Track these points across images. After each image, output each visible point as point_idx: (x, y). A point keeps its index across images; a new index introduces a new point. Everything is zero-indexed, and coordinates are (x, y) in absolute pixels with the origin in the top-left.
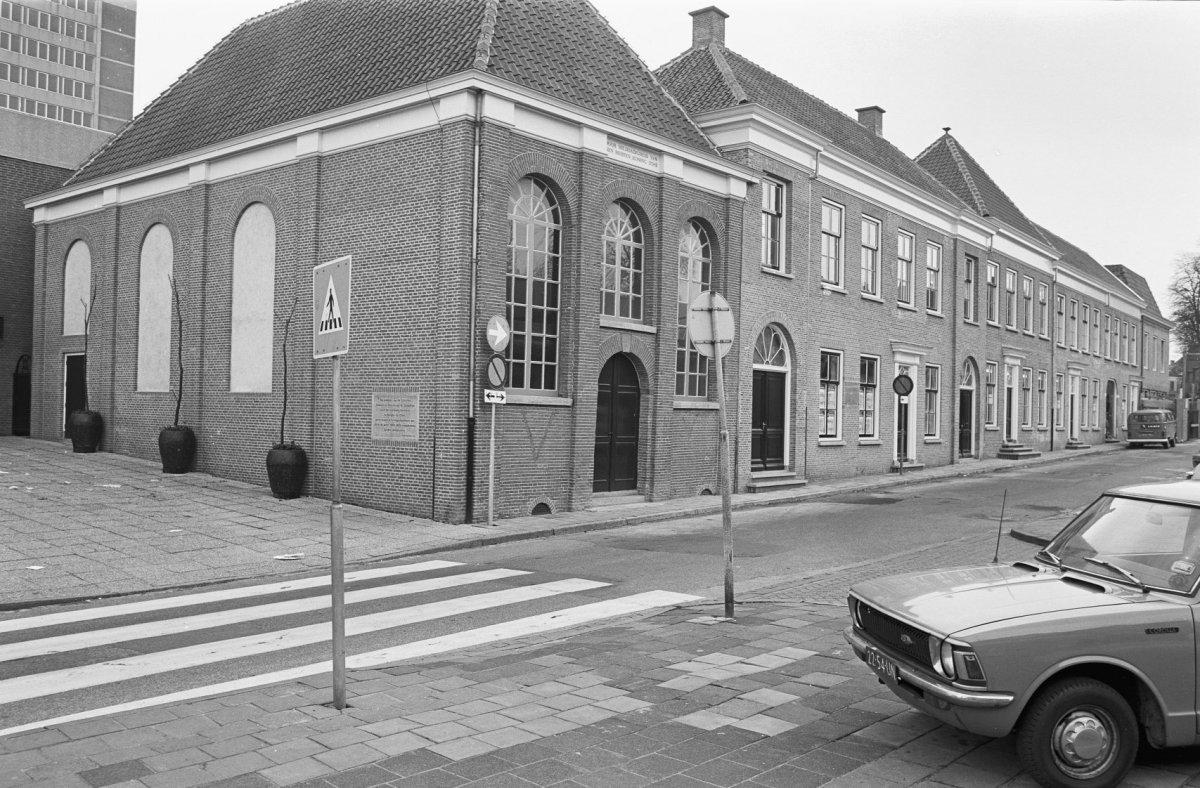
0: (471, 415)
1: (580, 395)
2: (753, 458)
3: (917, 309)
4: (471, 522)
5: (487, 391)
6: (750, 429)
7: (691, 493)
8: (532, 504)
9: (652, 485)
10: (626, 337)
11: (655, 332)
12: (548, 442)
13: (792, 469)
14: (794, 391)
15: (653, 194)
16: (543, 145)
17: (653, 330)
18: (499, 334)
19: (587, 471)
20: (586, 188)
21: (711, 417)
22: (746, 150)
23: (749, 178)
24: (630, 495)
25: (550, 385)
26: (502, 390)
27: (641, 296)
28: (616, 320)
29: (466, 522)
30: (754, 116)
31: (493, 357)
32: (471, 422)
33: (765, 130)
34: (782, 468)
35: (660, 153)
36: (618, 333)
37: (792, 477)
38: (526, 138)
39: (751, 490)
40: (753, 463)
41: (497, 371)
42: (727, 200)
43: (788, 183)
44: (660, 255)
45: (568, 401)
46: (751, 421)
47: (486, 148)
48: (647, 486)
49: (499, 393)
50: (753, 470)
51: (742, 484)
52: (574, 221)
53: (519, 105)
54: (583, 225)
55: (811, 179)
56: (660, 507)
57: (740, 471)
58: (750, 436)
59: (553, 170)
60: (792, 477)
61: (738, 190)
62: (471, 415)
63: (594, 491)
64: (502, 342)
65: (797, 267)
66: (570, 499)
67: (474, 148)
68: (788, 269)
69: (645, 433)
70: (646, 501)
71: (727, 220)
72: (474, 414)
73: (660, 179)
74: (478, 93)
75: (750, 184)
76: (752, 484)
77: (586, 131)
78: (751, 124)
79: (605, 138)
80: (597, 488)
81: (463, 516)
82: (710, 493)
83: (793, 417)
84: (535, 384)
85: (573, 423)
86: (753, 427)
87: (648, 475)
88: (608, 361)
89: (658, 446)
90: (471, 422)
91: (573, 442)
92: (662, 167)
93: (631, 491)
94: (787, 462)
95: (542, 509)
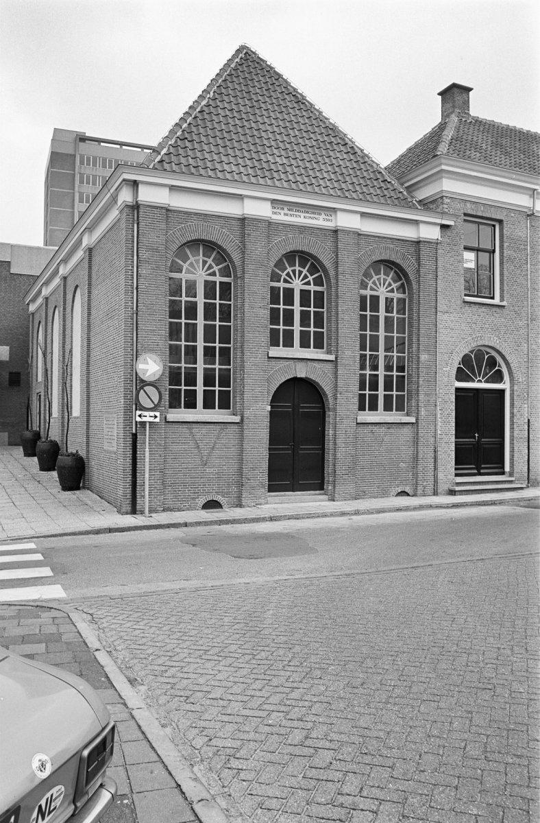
0: (134, 431)
1: (247, 413)
2: (456, 464)
3: (504, 303)
4: (437, 495)
5: (138, 413)
6: (453, 439)
7: (384, 494)
8: (202, 501)
9: (334, 487)
10: (300, 365)
11: (334, 359)
12: (217, 452)
13: (511, 474)
14: (512, 405)
15: (329, 244)
16: (205, 217)
17: (332, 357)
18: (151, 367)
19: (260, 473)
20: (249, 246)
21: (407, 431)
22: (442, 197)
23: (439, 221)
24: (316, 494)
25: (400, 408)
26: (155, 411)
27: (325, 330)
28: (297, 351)
29: (434, 495)
30: (444, 167)
31: (144, 386)
32: (135, 436)
33: (502, 187)
34: (503, 473)
35: (334, 210)
36: (291, 362)
37: (511, 482)
38: (186, 213)
39: (452, 493)
40: (456, 469)
41: (149, 397)
42: (418, 242)
43: (500, 222)
44: (337, 296)
45: (237, 419)
46: (454, 432)
47: (142, 224)
48: (330, 488)
49: (152, 414)
50: (457, 475)
51: (443, 487)
52: (239, 274)
53: (363, 215)
54: (246, 276)
55: (528, 216)
56: (339, 506)
57: (441, 476)
58: (454, 444)
59: (214, 234)
60: (511, 482)
61: (432, 233)
62: (134, 431)
63: (269, 492)
64: (154, 374)
65: (512, 295)
66: (239, 497)
67: (133, 226)
68: (502, 299)
69: (329, 445)
70: (329, 500)
71: (418, 260)
72: (136, 430)
73: (336, 231)
74: (135, 184)
75: (444, 227)
76: (452, 488)
77: (339, 214)
78: (444, 175)
79: (358, 217)
80: (272, 489)
81: (129, 509)
82: (408, 495)
83: (512, 429)
84: (388, 407)
85: (242, 439)
86: (456, 438)
87: (331, 479)
88: (281, 385)
89: (339, 455)
90: (135, 436)
91: (242, 451)
92: (336, 222)
93: (318, 492)
94: (507, 468)
95: (212, 505)
